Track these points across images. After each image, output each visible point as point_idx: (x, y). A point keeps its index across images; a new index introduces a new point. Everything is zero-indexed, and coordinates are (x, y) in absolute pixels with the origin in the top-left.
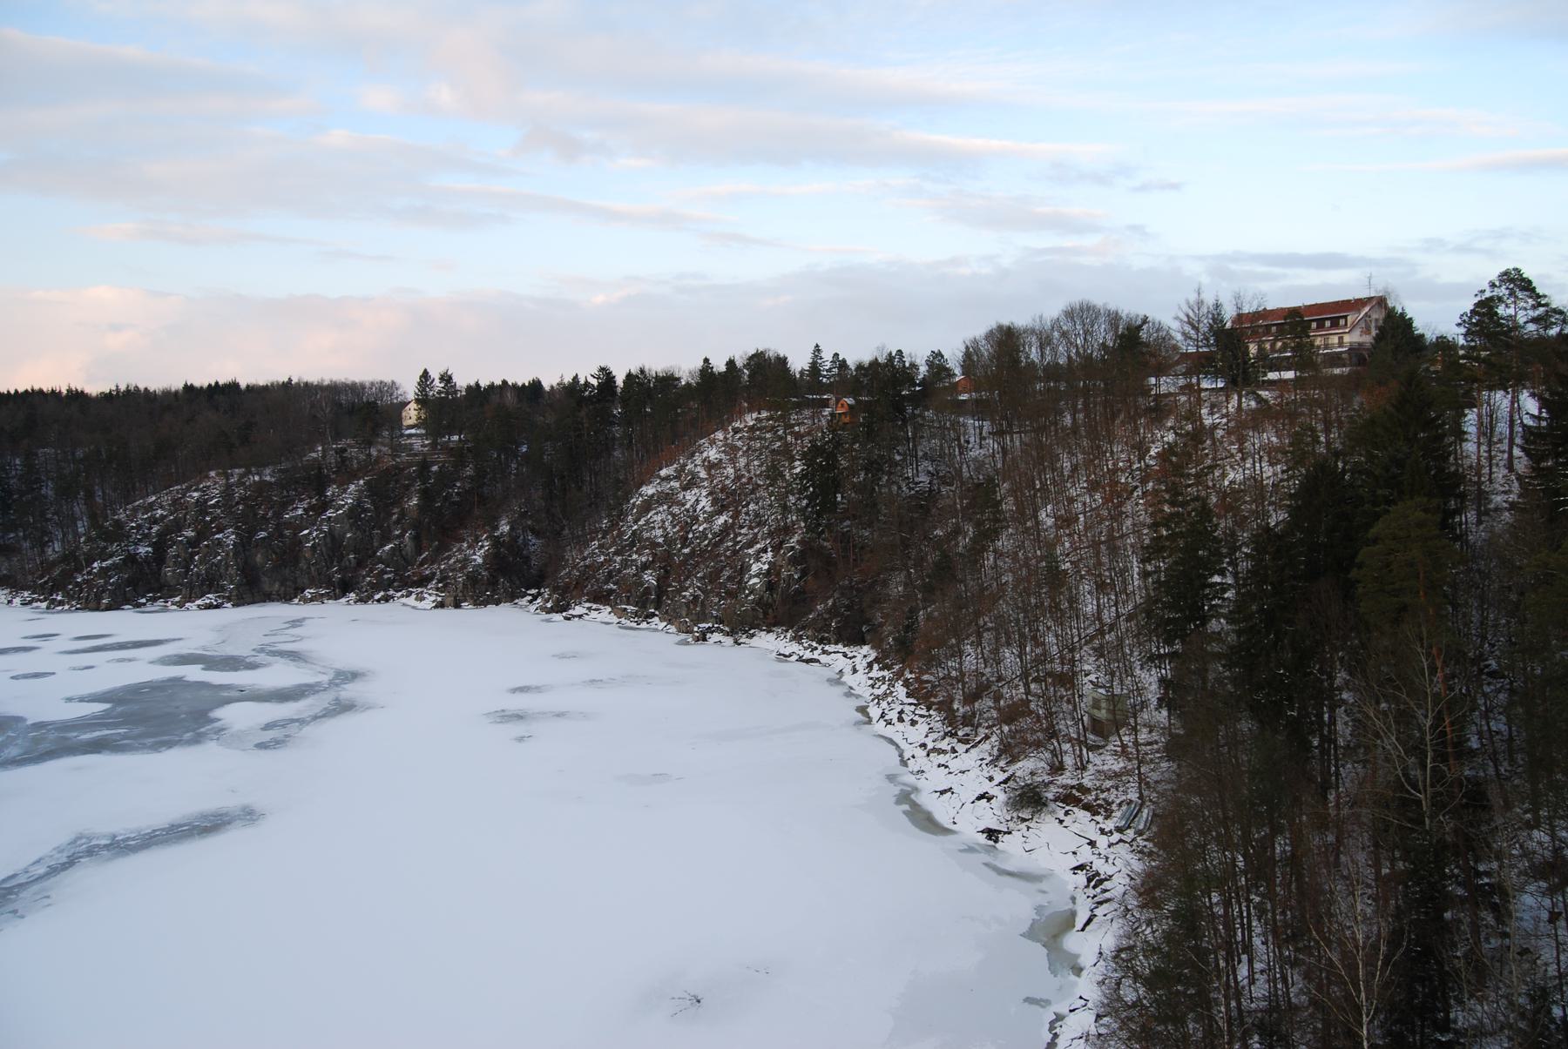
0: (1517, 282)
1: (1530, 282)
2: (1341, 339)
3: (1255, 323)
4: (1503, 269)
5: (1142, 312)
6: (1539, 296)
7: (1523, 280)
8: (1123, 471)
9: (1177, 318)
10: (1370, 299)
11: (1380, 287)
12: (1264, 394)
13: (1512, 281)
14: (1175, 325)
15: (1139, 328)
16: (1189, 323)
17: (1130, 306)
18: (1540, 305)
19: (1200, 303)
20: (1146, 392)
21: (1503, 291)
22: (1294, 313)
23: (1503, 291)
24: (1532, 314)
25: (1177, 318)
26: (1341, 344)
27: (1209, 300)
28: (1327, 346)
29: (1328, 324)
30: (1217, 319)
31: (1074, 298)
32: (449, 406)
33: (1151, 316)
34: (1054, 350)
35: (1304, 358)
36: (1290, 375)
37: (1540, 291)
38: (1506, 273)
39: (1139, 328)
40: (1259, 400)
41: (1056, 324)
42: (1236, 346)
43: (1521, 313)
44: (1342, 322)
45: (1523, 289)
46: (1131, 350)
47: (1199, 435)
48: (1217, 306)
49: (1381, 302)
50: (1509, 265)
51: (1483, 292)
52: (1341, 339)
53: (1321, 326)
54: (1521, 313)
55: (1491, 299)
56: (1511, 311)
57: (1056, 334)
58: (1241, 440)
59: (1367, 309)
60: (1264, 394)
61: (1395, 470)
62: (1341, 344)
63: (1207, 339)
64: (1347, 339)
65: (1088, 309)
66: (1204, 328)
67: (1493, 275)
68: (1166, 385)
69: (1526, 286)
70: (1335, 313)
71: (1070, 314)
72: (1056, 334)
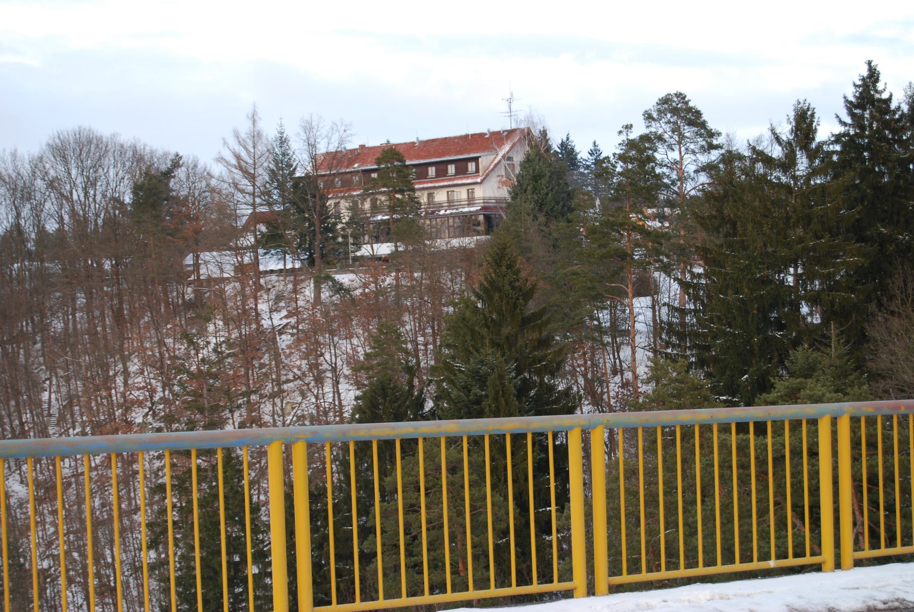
0: (680, 112)
1: (698, 113)
2: (470, 193)
3: (339, 167)
4: (662, 95)
5: (173, 150)
6: (711, 134)
7: (690, 110)
8: (140, 404)
9: (221, 160)
10: (511, 132)
11: (522, 116)
12: (345, 279)
13: (675, 111)
14: (217, 170)
15: (168, 174)
16: (245, 172)
17: (160, 141)
18: (712, 147)
19: (256, 136)
20: (182, 277)
21: (661, 127)
22: (391, 155)
23: (661, 127)
24: (703, 159)
25: (221, 160)
26: (471, 201)
27: (270, 132)
28: (451, 203)
29: (451, 169)
30: (282, 166)
31: (67, 123)
32: (568, 471)
33: (187, 152)
34: (37, 211)
35: (406, 226)
36: (384, 249)
37: (712, 125)
38: (666, 101)
39: (168, 174)
40: (338, 288)
41: (37, 164)
42: (312, 206)
43: (688, 158)
44: (471, 167)
45: (691, 123)
46: (157, 211)
47: (254, 344)
48: (283, 141)
49: (527, 135)
50: (670, 88)
51: (629, 127)
52: (470, 193)
53: (442, 172)
54: (688, 158)
55: (645, 138)
56: (674, 155)
57: (40, 184)
58: (313, 353)
59: (507, 148)
60: (345, 279)
61: (476, 390)
62: (471, 201)
63: (269, 193)
64: (479, 193)
65: (90, 142)
66: (263, 176)
67: (650, 104)
68: (215, 264)
69: (694, 118)
70: (457, 155)
71: (60, 151)
72: (40, 184)
